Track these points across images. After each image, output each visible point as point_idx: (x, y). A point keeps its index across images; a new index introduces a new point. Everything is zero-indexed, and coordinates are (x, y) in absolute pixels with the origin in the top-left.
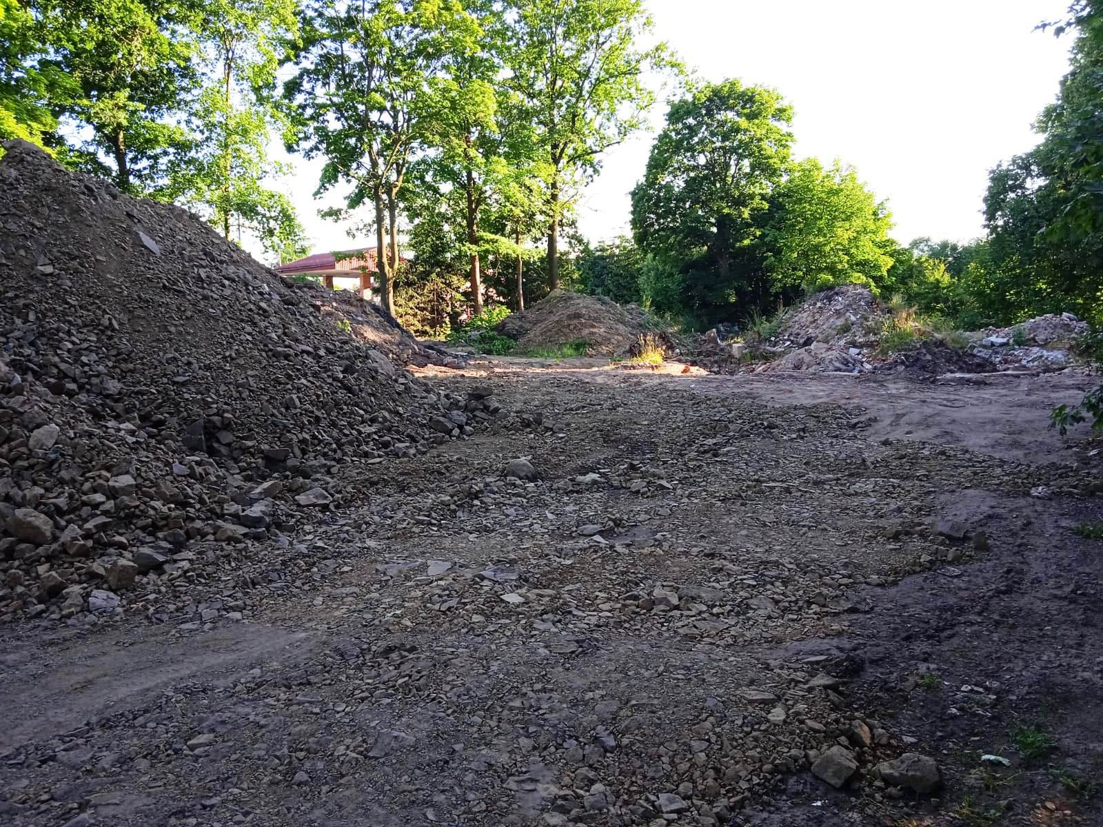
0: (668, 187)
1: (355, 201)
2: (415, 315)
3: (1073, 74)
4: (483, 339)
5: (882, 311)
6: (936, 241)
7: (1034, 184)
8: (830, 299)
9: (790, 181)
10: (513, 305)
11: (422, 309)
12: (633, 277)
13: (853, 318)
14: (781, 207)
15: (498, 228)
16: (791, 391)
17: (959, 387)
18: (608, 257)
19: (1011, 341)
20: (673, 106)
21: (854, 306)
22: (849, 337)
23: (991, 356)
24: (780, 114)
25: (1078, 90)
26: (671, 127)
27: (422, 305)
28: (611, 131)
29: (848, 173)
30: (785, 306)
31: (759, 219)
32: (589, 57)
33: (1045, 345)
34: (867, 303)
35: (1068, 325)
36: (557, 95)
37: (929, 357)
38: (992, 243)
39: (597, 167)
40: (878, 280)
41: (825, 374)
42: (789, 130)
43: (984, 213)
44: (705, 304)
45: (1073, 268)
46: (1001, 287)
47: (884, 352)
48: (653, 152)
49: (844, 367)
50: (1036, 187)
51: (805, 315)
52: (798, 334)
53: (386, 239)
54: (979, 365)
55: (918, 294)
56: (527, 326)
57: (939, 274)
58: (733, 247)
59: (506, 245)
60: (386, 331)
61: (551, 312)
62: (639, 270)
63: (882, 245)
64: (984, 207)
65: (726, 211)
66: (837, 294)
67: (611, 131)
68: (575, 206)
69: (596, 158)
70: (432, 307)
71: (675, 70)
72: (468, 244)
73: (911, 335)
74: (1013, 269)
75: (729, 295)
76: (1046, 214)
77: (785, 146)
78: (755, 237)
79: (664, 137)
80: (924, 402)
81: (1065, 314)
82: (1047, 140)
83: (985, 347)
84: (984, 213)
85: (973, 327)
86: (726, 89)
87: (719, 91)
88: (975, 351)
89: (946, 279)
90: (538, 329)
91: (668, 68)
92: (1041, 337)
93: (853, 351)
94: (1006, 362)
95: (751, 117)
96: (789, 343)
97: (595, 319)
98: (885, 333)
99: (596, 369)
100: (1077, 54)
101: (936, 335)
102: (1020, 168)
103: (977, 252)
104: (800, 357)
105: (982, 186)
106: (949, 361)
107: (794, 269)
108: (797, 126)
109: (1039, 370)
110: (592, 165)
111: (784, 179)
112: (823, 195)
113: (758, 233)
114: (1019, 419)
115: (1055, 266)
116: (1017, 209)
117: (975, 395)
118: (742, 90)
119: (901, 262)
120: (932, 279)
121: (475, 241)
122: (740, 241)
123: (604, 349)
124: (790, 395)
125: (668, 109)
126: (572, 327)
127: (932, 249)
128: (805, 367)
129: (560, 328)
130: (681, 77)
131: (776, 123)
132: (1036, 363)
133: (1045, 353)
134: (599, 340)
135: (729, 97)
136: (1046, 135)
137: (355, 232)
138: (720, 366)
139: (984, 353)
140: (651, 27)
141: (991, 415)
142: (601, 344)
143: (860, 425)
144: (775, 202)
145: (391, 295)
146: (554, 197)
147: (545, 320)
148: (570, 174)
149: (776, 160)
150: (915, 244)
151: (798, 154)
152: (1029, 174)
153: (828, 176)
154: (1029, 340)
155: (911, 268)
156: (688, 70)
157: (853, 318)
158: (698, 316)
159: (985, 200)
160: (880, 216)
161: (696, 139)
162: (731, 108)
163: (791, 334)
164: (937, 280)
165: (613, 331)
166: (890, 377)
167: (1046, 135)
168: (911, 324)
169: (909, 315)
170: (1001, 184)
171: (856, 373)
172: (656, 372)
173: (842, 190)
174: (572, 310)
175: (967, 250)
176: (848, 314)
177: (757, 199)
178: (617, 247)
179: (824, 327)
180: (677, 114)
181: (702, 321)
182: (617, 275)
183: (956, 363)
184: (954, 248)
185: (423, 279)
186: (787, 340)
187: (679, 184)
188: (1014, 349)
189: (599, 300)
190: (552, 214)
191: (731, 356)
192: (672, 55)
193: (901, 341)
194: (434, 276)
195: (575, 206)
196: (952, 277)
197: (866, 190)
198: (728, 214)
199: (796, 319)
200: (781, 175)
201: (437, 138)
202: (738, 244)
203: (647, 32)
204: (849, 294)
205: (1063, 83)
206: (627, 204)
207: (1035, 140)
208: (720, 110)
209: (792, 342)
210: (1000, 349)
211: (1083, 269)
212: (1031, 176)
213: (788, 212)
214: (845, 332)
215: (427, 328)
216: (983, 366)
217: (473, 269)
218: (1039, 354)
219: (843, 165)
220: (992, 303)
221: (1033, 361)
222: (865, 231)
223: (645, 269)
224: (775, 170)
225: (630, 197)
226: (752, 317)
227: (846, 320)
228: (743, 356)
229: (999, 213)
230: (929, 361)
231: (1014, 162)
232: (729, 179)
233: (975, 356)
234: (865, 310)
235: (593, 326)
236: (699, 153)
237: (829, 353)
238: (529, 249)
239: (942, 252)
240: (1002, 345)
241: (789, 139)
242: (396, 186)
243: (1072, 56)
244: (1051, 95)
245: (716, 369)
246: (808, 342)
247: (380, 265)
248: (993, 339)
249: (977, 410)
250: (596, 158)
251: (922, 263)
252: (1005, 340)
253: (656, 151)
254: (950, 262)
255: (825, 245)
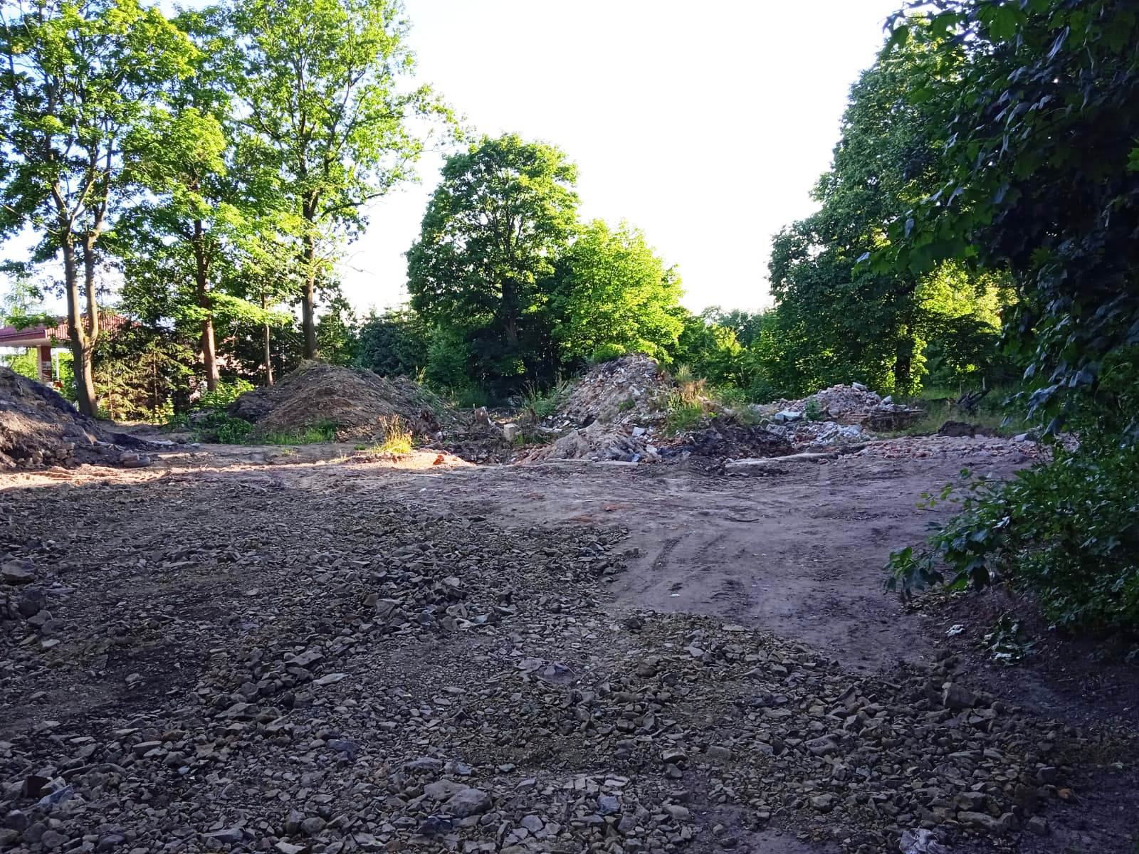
0: (449, 247)
1: (44, 253)
2: (125, 394)
3: (845, 142)
4: (210, 422)
5: (668, 383)
6: (727, 311)
7: (815, 251)
8: (612, 371)
9: (577, 243)
10: (258, 379)
11: (135, 386)
12: (424, 347)
13: (637, 393)
14: (569, 271)
15: (238, 288)
16: (541, 498)
17: (752, 480)
18: (396, 325)
19: (804, 415)
20: (448, 159)
21: (638, 379)
22: (633, 414)
23: (784, 433)
24: (563, 173)
25: (851, 157)
26: (448, 183)
27: (135, 381)
28: (372, 181)
29: (634, 236)
30: (563, 379)
31: (546, 284)
32: (340, 94)
33: (839, 419)
34: (652, 375)
35: (859, 396)
36: (306, 138)
37: (719, 436)
38: (782, 309)
39: (361, 223)
40: (670, 348)
41: (598, 464)
42: (574, 190)
43: (770, 279)
44: (493, 376)
45: (857, 335)
46: (791, 356)
47: (671, 432)
48: (429, 209)
49: (623, 454)
50: (817, 254)
51: (585, 389)
52: (578, 412)
53: (80, 302)
54: (772, 443)
55: (710, 364)
56: (269, 404)
57: (730, 343)
58: (520, 315)
59: (245, 308)
60: (46, 418)
61: (300, 388)
62: (430, 338)
63: (675, 312)
64: (769, 273)
65: (509, 274)
66: (620, 365)
67: (372, 181)
68: (334, 265)
69: (361, 211)
70: (151, 384)
71: (443, 117)
72: (194, 307)
73: (700, 411)
74: (801, 337)
75: (517, 366)
76: (829, 280)
77: (570, 207)
78: (542, 304)
79: (441, 191)
80: (706, 514)
81: (855, 384)
82: (825, 207)
83: (777, 422)
84: (770, 279)
85: (764, 399)
86: (505, 144)
87: (497, 145)
88: (768, 428)
89: (737, 348)
90: (280, 409)
91: (435, 114)
92: (834, 410)
93: (638, 431)
94: (801, 439)
95: (533, 174)
96: (567, 422)
97: (351, 396)
98: (671, 409)
99: (322, 463)
100: (847, 123)
101: (727, 410)
102: (802, 233)
103: (766, 321)
104: (574, 441)
105: (766, 252)
106: (741, 440)
107: (585, 338)
108: (582, 187)
109: (837, 451)
110: (356, 220)
111: (570, 242)
112: (610, 259)
113: (545, 299)
114: (830, 544)
115: (840, 334)
116: (801, 275)
117: (768, 498)
118: (522, 145)
119: (693, 331)
120: (723, 348)
121: (208, 303)
122: (527, 308)
123: (360, 431)
124: (538, 504)
125: (444, 164)
126: (321, 405)
127: (722, 318)
128: (578, 454)
129: (308, 406)
130: (449, 124)
131: (560, 183)
132: (831, 440)
133: (840, 428)
134: (354, 421)
135: (509, 152)
136: (824, 202)
137: (43, 292)
138: (489, 452)
139: (777, 430)
140: (411, 66)
141: (790, 536)
142: (356, 425)
143: (609, 570)
144: (562, 266)
145: (88, 370)
146: (308, 253)
147: (291, 397)
148: (323, 227)
149: (559, 221)
150: (707, 313)
151: (584, 216)
152: (811, 241)
153: (614, 239)
154: (822, 413)
155: (703, 336)
156: (457, 118)
157: (637, 393)
158: (487, 390)
159: (770, 266)
160: (670, 282)
161: (475, 197)
162: (512, 165)
163: (570, 412)
164: (728, 348)
165: (373, 410)
166: (672, 468)
167: (824, 202)
168: (699, 397)
169: (697, 388)
170: (785, 251)
171: (634, 463)
172: (399, 465)
173: (629, 254)
174: (324, 385)
175: (757, 319)
176: (631, 387)
177: (543, 263)
178: (405, 314)
179: (606, 403)
180: (454, 168)
181: (490, 395)
182: (405, 344)
183: (747, 442)
184: (744, 317)
185: (137, 349)
186: (566, 419)
187: (460, 244)
188: (808, 424)
189: (359, 372)
190: (304, 273)
191: (502, 439)
192: (438, 100)
193: (689, 419)
194: (151, 345)
195: (334, 265)
196: (743, 346)
197: (654, 256)
198: (512, 278)
199: (576, 393)
200: (566, 238)
201: (147, 177)
202: (524, 311)
203: (408, 72)
204: (633, 365)
205: (836, 151)
206: (404, 264)
207: (815, 208)
208: (500, 167)
209: (571, 421)
210: (793, 425)
211: (867, 337)
212: (813, 243)
213: (575, 276)
214: (629, 409)
215: (143, 410)
216: (777, 446)
217: (206, 335)
218: (834, 430)
219: (629, 226)
220: (783, 372)
221: (828, 437)
222: (655, 298)
223: (435, 338)
224: (560, 232)
225: (405, 258)
226: (526, 392)
227: (630, 395)
228: (516, 439)
229: (785, 279)
230: (720, 441)
231: (795, 227)
232: (514, 241)
233: (768, 433)
234: (650, 383)
235: (348, 405)
236: (480, 212)
237: (607, 436)
238: (282, 311)
239: (731, 322)
240: (795, 419)
241: (573, 199)
242: (93, 235)
243: (843, 125)
244: (825, 163)
245: (484, 456)
246: (587, 422)
247: (73, 332)
248: (786, 413)
249: (771, 526)
250: (361, 211)
251: (713, 331)
252: (797, 414)
253: (433, 209)
254: (741, 331)
255: (614, 312)
